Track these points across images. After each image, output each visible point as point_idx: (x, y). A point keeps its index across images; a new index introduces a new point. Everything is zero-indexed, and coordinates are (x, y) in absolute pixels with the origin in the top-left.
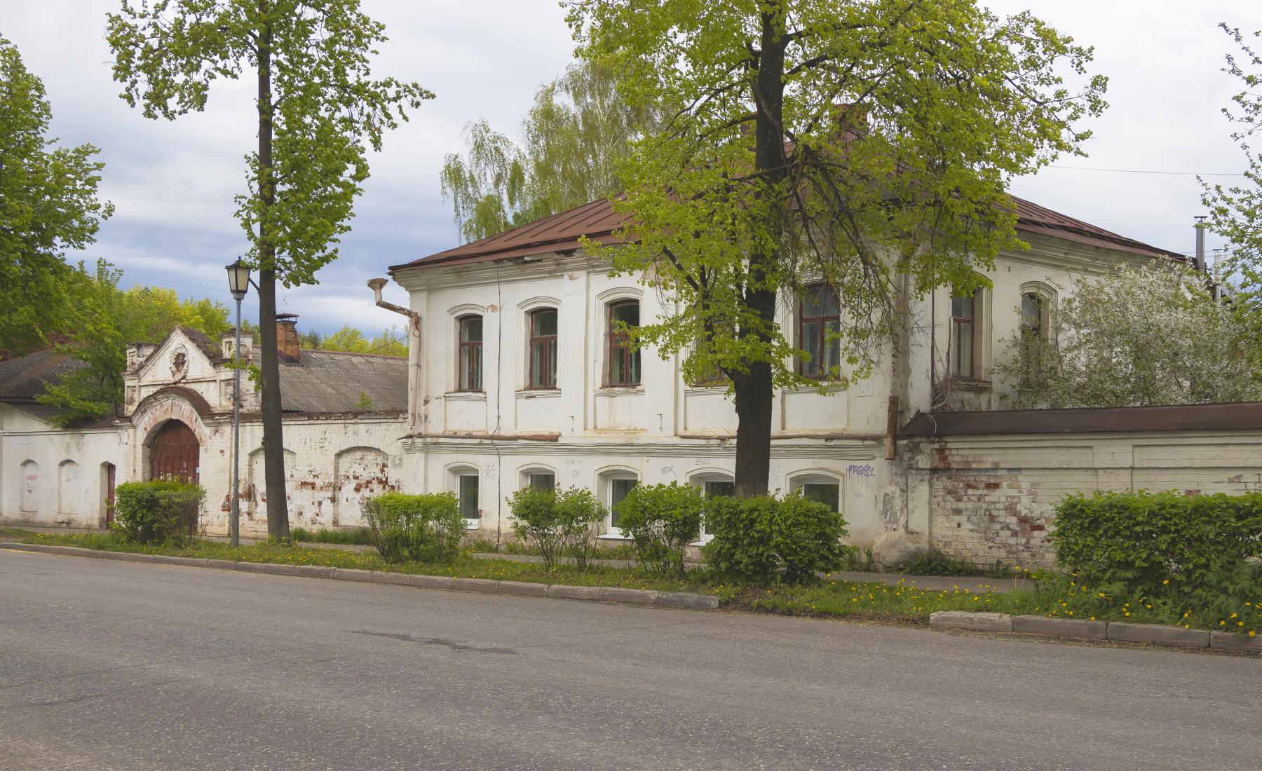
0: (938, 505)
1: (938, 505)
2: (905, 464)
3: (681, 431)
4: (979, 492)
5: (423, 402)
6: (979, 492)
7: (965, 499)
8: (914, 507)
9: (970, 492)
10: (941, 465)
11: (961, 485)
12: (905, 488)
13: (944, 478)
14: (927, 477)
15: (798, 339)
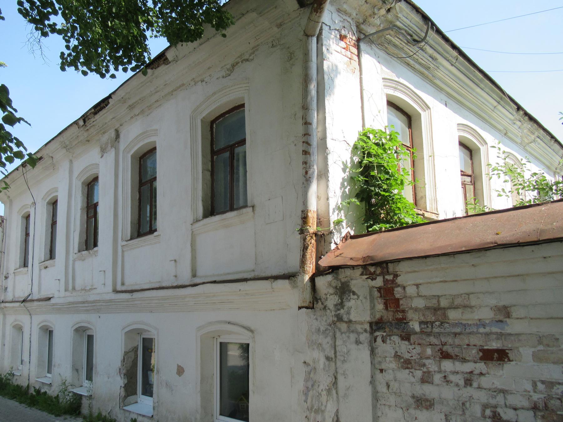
0: (388, 386)
1: (388, 386)
2: (330, 316)
3: (119, 288)
4: (468, 367)
5: (4, 278)
6: (468, 367)
7: (437, 378)
8: (348, 389)
9: (447, 365)
10: (389, 316)
11: (429, 351)
12: (332, 355)
13: (396, 338)
14: (365, 337)
15: (208, 174)
